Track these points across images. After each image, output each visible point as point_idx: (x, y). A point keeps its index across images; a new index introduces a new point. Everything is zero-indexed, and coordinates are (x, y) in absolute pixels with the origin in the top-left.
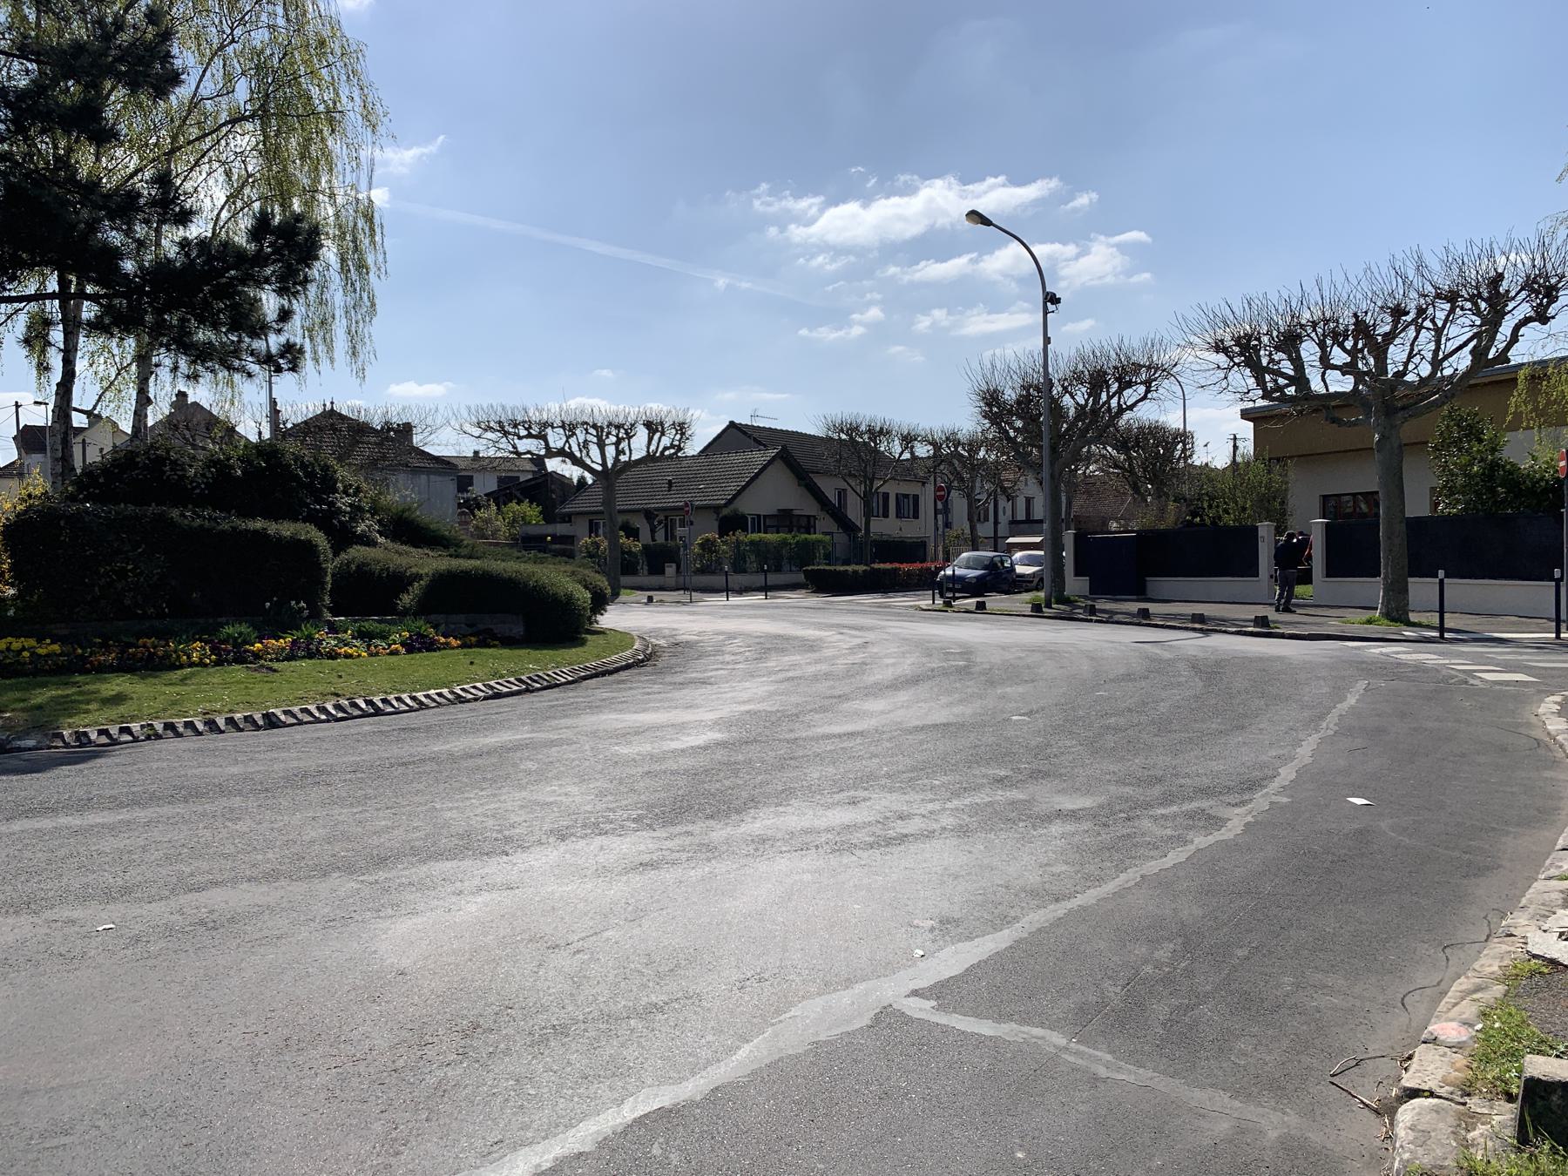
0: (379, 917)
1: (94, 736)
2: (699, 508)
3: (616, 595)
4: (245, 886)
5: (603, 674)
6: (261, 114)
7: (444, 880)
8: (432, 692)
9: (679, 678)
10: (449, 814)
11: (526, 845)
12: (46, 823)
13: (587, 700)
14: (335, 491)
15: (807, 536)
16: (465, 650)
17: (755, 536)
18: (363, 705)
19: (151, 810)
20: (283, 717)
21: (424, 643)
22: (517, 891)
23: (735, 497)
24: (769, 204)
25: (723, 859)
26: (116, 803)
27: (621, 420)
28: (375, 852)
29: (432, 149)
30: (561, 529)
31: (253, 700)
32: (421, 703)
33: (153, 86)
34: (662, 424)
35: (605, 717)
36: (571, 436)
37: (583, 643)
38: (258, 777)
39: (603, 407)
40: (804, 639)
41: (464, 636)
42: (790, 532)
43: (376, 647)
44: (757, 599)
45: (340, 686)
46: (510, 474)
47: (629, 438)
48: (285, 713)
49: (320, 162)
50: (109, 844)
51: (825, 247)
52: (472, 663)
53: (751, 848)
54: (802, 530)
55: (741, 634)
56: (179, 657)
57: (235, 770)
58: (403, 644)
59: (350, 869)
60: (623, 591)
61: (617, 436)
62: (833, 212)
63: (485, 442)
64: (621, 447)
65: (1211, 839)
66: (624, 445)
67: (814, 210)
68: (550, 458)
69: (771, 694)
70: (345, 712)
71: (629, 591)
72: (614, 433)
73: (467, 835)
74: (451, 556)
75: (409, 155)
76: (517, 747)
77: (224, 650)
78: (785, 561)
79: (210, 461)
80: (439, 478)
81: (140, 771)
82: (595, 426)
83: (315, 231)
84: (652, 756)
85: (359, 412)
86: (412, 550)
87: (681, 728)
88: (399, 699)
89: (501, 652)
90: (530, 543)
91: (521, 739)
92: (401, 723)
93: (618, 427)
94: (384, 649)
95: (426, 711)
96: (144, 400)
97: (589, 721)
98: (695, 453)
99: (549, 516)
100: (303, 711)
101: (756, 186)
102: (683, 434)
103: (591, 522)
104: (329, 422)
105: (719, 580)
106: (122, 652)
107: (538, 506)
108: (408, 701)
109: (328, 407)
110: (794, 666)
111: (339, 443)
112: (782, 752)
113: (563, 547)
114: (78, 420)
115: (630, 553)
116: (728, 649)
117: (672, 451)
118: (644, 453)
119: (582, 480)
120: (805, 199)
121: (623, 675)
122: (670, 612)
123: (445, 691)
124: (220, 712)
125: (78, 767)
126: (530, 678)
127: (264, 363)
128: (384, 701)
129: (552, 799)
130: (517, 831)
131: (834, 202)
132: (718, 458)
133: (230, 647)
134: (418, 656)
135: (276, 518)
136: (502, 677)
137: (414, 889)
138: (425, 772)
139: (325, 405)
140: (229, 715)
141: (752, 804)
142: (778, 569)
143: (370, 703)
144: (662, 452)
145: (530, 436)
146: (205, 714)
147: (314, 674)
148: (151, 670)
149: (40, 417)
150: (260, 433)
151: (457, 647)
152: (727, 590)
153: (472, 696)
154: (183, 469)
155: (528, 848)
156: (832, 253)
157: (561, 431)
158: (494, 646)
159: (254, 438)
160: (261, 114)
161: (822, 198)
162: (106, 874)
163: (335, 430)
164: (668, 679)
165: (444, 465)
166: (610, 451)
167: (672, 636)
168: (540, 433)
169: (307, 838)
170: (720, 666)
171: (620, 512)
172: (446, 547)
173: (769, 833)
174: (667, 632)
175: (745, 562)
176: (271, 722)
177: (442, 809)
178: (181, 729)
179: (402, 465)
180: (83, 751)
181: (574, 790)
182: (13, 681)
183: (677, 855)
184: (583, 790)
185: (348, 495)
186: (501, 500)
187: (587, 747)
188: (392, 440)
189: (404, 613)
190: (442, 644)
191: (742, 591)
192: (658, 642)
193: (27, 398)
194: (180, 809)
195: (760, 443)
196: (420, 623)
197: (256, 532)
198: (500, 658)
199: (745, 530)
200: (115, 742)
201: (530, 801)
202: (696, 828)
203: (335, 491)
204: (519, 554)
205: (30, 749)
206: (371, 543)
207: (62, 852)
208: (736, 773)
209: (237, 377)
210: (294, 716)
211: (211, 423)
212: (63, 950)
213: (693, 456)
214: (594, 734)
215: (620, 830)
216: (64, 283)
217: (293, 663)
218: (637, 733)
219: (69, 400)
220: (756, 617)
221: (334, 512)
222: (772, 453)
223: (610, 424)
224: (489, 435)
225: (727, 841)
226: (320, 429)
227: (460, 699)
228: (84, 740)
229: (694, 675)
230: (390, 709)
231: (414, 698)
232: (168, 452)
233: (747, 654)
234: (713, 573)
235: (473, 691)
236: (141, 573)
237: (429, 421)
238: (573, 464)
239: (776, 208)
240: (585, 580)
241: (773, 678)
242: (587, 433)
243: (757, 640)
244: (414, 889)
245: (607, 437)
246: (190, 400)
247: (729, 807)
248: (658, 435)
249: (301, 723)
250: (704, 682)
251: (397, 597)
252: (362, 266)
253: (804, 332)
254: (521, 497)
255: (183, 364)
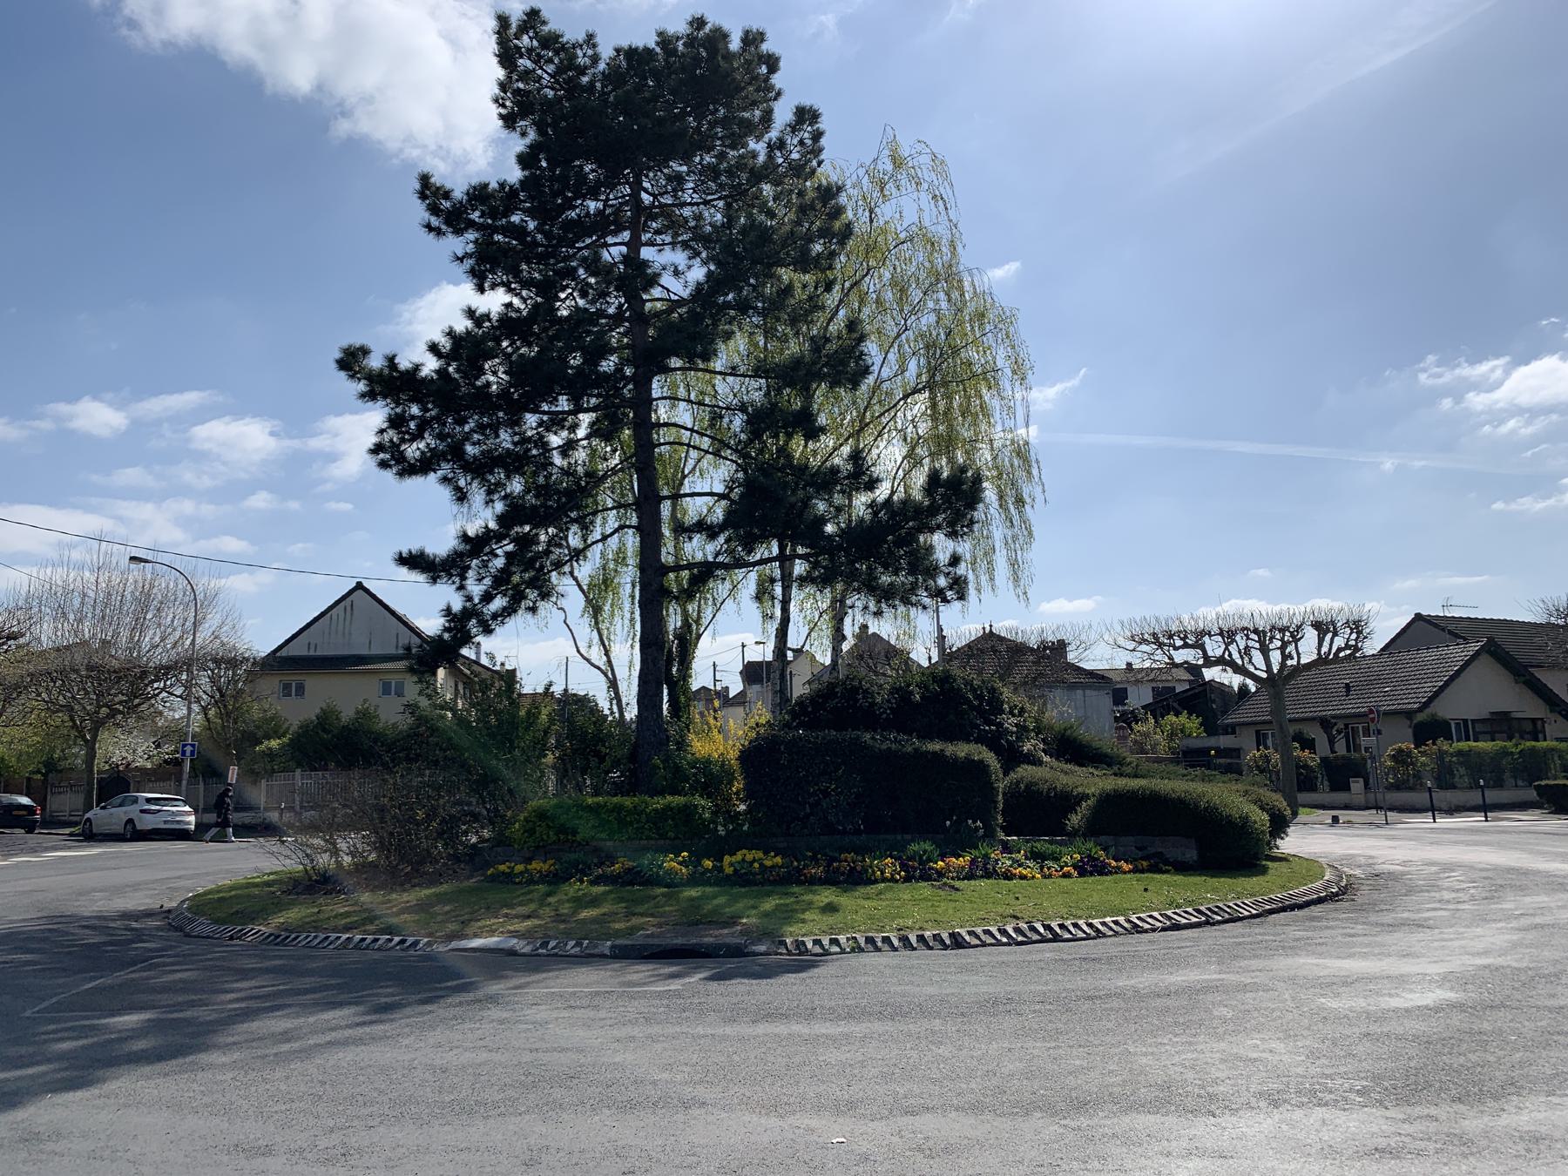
0: (1086, 1169)
1: (810, 945)
2: (1386, 713)
3: (1295, 814)
4: (953, 1114)
5: (1292, 908)
6: (931, 386)
7: (1149, 1136)
8: (1108, 919)
9: (1388, 918)
10: (1144, 1060)
11: (1234, 1106)
12: (781, 1029)
13: (1278, 938)
14: (1002, 712)
15: (1533, 743)
16: (1138, 875)
17: (1463, 745)
18: (1042, 930)
19: (864, 1025)
20: (967, 938)
21: (1096, 866)
22: (1231, 1161)
23: (1431, 700)
24: (1440, 376)
25: (1484, 1157)
26: (834, 1015)
27: (1285, 622)
28: (1074, 1095)
29: (1075, 382)
30: (1225, 741)
31: (939, 919)
32: (1098, 931)
33: (850, 381)
34: (1333, 622)
35: (1302, 961)
36: (1231, 643)
37: (1263, 871)
38: (953, 1000)
39: (1260, 608)
40: (1547, 874)
41: (1136, 860)
42: (1510, 738)
43: (1049, 869)
44: (1475, 820)
45: (1017, 909)
46: (1167, 685)
47: (1296, 641)
48: (970, 933)
49: (976, 414)
50: (833, 1056)
51: (1516, 411)
52: (1146, 890)
53: (1521, 1147)
54: (1526, 736)
55: (1460, 866)
56: (874, 872)
57: (931, 990)
58: (1075, 867)
59: (1051, 1110)
60: (1301, 810)
61: (1282, 640)
62: (1523, 370)
63: (1139, 654)
64: (1287, 651)
65: (1544, 504)
66: (1291, 649)
67: (1499, 373)
68: (1209, 667)
69: (1515, 946)
70: (1025, 936)
71: (1308, 810)
72: (1278, 637)
73: (1167, 1086)
74: (1115, 775)
75: (1052, 392)
76: (1208, 988)
77: (913, 867)
78: (1507, 774)
79: (893, 688)
80: (1094, 693)
81: (851, 985)
82: (1256, 631)
83: (978, 479)
84: (1368, 1015)
85: (1011, 633)
86: (1077, 768)
87: (1401, 981)
88: (1076, 925)
89: (1175, 878)
90: (1193, 758)
91: (1207, 981)
92: (1081, 951)
93: (1283, 630)
94: (1056, 871)
95: (1102, 940)
96: (838, 637)
97: (1285, 964)
98: (1375, 652)
99: (1211, 728)
100: (986, 932)
101: (1421, 359)
102: (1359, 633)
103: (1258, 732)
104: (990, 643)
105: (1421, 798)
106: (829, 865)
107: (1198, 717)
108: (1085, 928)
109: (987, 631)
110: (1542, 910)
111: (1000, 663)
112: (1544, 1023)
113: (1229, 761)
114: (790, 655)
115: (1306, 766)
116: (1446, 884)
117: (1348, 652)
118: (1315, 657)
119: (1243, 687)
120: (1484, 363)
121: (1316, 910)
122: (1362, 836)
123: (1121, 919)
124: (911, 929)
125: (800, 975)
126: (1209, 909)
127: (936, 596)
128: (1062, 926)
129: (1255, 1055)
130: (1221, 1088)
131: (1525, 359)
132: (1405, 656)
133: (916, 864)
134: (1091, 879)
135: (950, 738)
136: (1178, 906)
137: (1119, 1142)
138: (1112, 1009)
139: (984, 628)
140: (920, 933)
141: (1513, 1090)
142: (1499, 784)
143: (1048, 928)
144: (1336, 654)
145: (1186, 646)
146: (899, 930)
147: (993, 894)
148: (851, 883)
149: (765, 653)
150: (930, 658)
151: (1130, 872)
152: (1433, 809)
153: (1149, 926)
154: (873, 697)
155: (1237, 1110)
156: (1527, 415)
157: (1220, 638)
158: (1167, 872)
159: (925, 664)
160: (931, 386)
161: (1507, 359)
162: (834, 1086)
163: (995, 651)
164: (1373, 918)
165: (1097, 679)
166: (1276, 657)
167: (1370, 865)
168: (1197, 642)
169: (1006, 1071)
170: (1438, 905)
171: (1290, 720)
172: (1110, 765)
173: (1543, 1129)
174: (1363, 861)
175: (1453, 776)
176: (958, 943)
177: (1135, 1054)
178: (879, 944)
179: (1058, 682)
180: (802, 960)
181: (1279, 1046)
182: (747, 889)
183: (1422, 1144)
184: (1289, 1048)
185: (1014, 716)
186: (1158, 712)
187: (1287, 996)
188: (1048, 657)
189: (1073, 834)
190: (1113, 868)
191: (1452, 811)
192: (1352, 872)
193: (750, 639)
194: (889, 1026)
195: (1457, 636)
196: (1090, 845)
197: (935, 753)
198: (1175, 885)
199: (1449, 737)
200: (826, 953)
201: (1231, 1055)
202: (1442, 1112)
203: (1002, 712)
204: (1185, 772)
205: (761, 954)
206: (1037, 762)
207: (797, 1059)
208: (1484, 1045)
209: (913, 611)
210: (978, 937)
211: (893, 653)
212: (807, 1158)
213: (1373, 655)
214: (1293, 980)
215: (1342, 1104)
216: (782, 548)
217: (973, 882)
218: (1345, 984)
219: (785, 642)
220: (1476, 844)
221: (1002, 731)
222: (1475, 647)
223: (1273, 628)
224: (1144, 647)
225: (1486, 1134)
226: (982, 651)
227: (1137, 929)
228: (803, 949)
229: (1405, 915)
230: (1068, 936)
231: (1090, 925)
232: (860, 683)
233: (1472, 891)
234: (1412, 789)
235: (1149, 920)
236: (841, 793)
237: (1083, 637)
238: (1235, 672)
239: (1448, 377)
240: (1260, 800)
241: (1514, 924)
242: (1248, 638)
243: (1484, 874)
244: (1119, 1142)
245: (1271, 642)
246: (871, 631)
247: (1480, 1090)
248: (1329, 635)
249: (984, 945)
250: (1420, 925)
251: (1066, 817)
252: (1020, 501)
253: (1498, 506)
254: (1180, 709)
255: (872, 606)
